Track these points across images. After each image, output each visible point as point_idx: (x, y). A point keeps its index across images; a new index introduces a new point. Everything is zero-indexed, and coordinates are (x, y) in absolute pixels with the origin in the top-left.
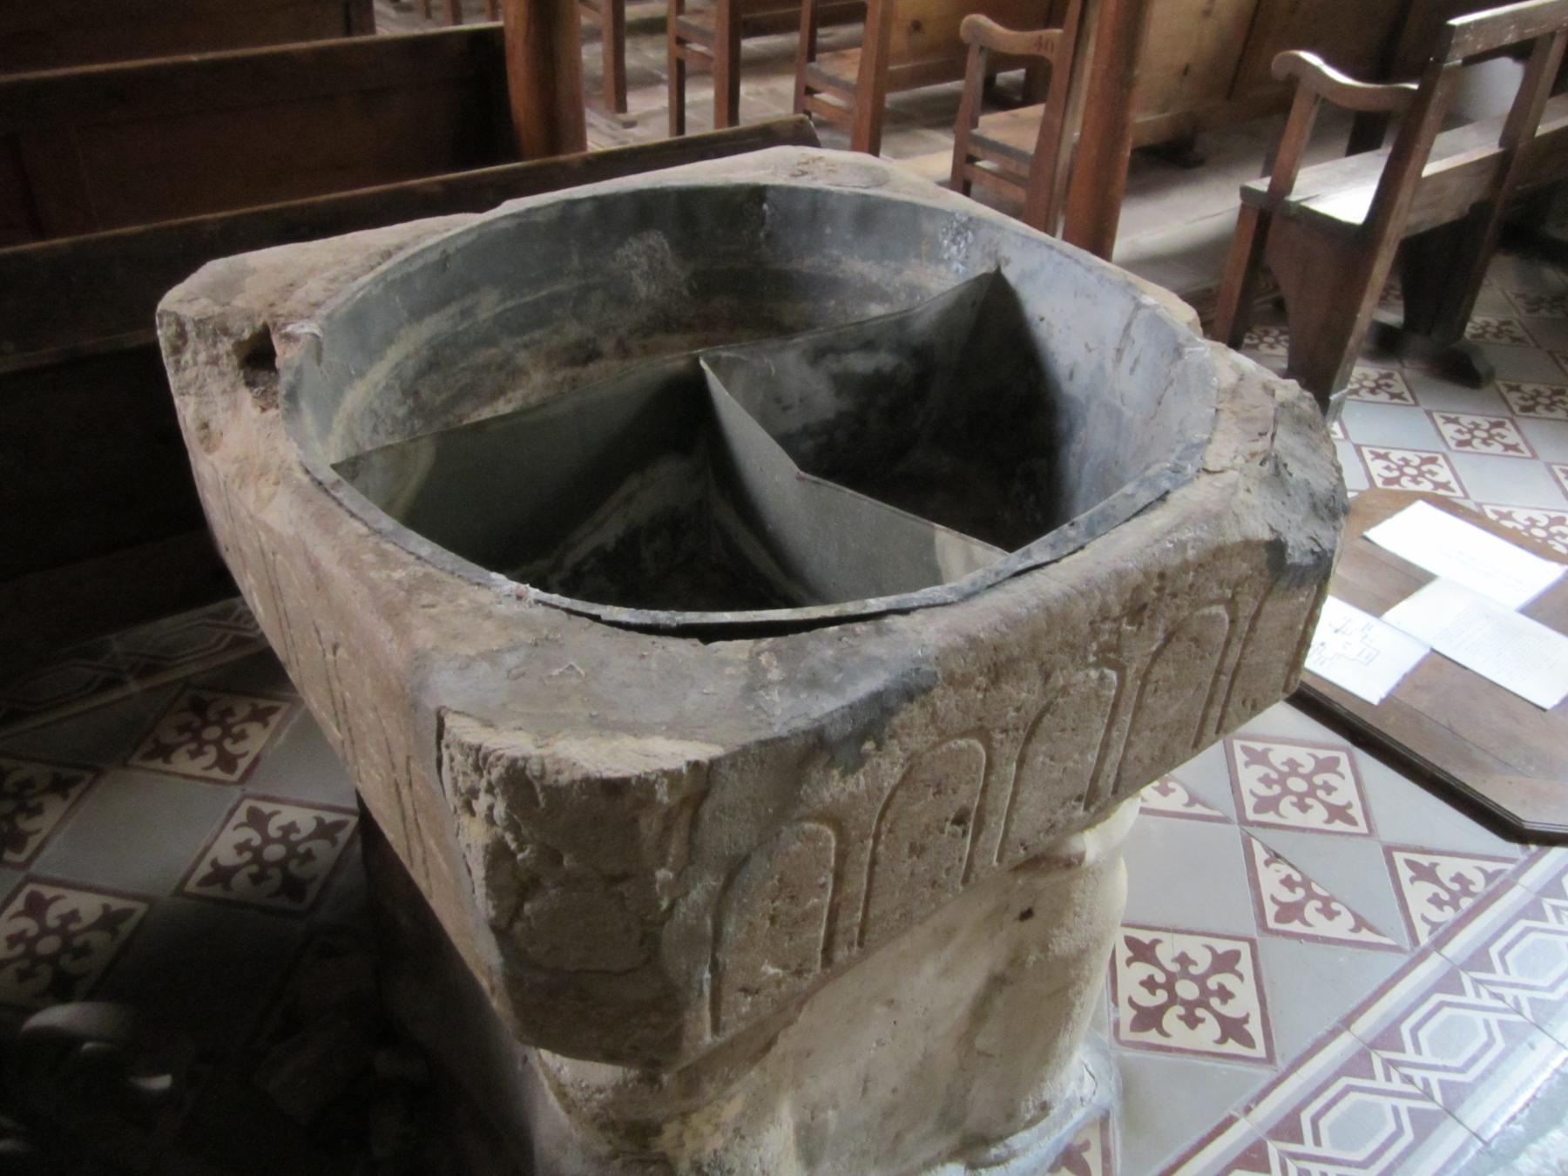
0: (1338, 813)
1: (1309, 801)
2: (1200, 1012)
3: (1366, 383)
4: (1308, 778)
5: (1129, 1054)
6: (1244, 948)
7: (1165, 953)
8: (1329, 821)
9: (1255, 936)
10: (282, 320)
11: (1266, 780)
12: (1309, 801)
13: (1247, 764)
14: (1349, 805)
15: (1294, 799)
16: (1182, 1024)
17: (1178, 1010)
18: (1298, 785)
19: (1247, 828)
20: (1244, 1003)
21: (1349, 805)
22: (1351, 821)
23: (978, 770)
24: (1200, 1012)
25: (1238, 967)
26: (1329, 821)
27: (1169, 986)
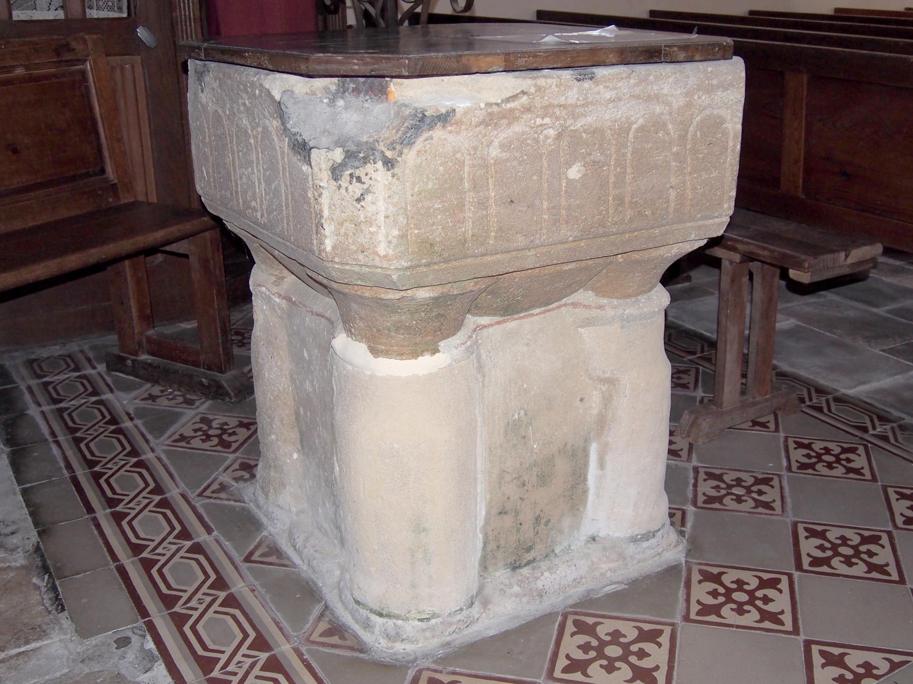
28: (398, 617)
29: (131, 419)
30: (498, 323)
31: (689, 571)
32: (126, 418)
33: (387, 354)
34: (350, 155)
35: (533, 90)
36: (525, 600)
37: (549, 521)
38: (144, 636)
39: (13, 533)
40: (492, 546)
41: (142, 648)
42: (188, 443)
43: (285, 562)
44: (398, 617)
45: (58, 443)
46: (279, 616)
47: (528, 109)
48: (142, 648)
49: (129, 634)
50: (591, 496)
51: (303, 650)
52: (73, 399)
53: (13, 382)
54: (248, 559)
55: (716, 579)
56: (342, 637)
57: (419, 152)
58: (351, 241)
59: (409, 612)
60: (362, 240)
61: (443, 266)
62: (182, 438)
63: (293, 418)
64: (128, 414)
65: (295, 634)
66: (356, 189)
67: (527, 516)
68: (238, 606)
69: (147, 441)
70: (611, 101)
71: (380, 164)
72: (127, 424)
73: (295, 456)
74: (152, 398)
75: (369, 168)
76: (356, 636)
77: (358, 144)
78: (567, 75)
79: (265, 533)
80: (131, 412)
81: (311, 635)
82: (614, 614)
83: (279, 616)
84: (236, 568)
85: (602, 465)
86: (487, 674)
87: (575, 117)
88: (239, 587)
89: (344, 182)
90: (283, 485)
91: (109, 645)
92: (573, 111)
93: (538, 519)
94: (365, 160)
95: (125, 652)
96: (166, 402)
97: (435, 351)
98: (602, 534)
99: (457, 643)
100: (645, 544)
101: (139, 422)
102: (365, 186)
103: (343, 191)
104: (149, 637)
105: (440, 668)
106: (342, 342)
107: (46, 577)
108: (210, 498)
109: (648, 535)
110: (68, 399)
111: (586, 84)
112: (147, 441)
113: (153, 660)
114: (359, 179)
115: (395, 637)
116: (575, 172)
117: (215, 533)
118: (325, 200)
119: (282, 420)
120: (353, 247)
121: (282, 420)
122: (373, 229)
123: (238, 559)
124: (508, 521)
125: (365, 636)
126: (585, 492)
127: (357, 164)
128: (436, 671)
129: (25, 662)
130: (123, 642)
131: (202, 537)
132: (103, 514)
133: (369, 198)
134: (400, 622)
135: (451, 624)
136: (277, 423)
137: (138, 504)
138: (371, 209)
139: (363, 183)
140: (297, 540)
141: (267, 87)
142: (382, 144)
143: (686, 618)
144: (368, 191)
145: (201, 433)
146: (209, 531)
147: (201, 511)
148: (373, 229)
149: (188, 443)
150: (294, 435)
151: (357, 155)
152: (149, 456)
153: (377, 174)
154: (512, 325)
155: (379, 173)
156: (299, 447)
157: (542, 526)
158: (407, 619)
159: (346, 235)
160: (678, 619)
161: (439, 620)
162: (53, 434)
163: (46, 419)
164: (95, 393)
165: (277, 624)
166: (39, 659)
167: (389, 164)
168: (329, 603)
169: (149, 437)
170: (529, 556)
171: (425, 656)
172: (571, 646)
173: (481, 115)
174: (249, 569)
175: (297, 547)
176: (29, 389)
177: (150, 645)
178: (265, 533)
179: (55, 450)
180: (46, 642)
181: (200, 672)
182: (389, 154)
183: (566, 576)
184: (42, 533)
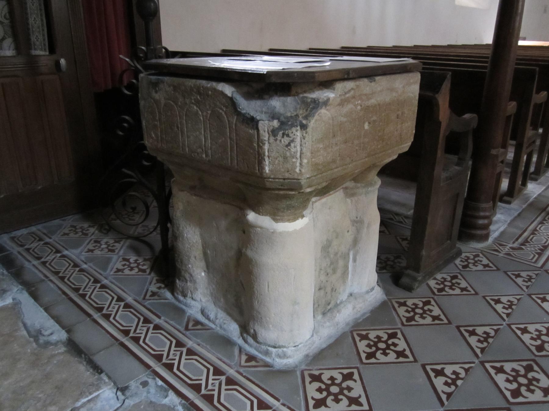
0: (401, 354)
1: (387, 351)
2: (340, 397)
3: (389, 263)
4: (386, 342)
5: (299, 374)
6: (355, 371)
7: (325, 378)
8: (397, 358)
9: (358, 366)
10: (18, 292)
11: (369, 346)
12: (387, 351)
13: (360, 341)
14: (404, 350)
15: (381, 352)
16: (334, 403)
17: (332, 397)
18: (382, 345)
19: (350, 334)
20: (357, 391)
21: (404, 350)
22: (407, 357)
23: (228, 159)
24: (340, 397)
25: (354, 378)
26: (397, 358)
27: (327, 389)
28: (284, 347)
29: (86, 263)
30: (319, 200)
31: (392, 303)
32: (81, 263)
33: (282, 220)
34: (282, 123)
35: (355, 87)
36: (332, 328)
37: (336, 290)
38: (155, 379)
39: (52, 334)
40: (316, 306)
41: (157, 386)
42: (123, 272)
43: (208, 328)
44: (284, 347)
45: (51, 281)
46: (220, 356)
47: (354, 97)
48: (157, 386)
49: (146, 379)
50: (350, 276)
51: (241, 370)
52: (47, 256)
53: (8, 251)
54: (187, 329)
55: (404, 304)
56: (257, 361)
57: (316, 120)
58: (281, 167)
59: (289, 343)
60: (289, 166)
61: (320, 175)
62: (118, 270)
63: (202, 255)
64: (83, 261)
65: (233, 364)
66: (286, 140)
67: (329, 289)
68: (195, 354)
69: (101, 274)
70: (381, 91)
71: (299, 128)
72: (84, 266)
73: (203, 274)
74: (92, 251)
75: (294, 129)
76: (262, 360)
77: (287, 118)
78: (366, 80)
79: (188, 314)
80: (84, 260)
81: (240, 363)
82: (372, 328)
83: (220, 356)
84: (183, 334)
85: (355, 260)
86: (334, 367)
87: (369, 99)
88: (190, 344)
89: (279, 137)
90: (196, 289)
91: (138, 387)
92: (368, 97)
93: (332, 289)
94: (293, 126)
95: (149, 389)
96: (99, 253)
97: (303, 216)
98: (355, 292)
99: (311, 354)
100: (371, 293)
101: (91, 264)
102: (291, 139)
103: (278, 142)
104: (157, 379)
105: (310, 368)
106: (252, 216)
107: (83, 356)
108: (150, 300)
109: (373, 289)
110: (45, 256)
111: (373, 84)
112: (101, 274)
113: (166, 391)
114: (288, 136)
115: (284, 356)
116: (366, 126)
117: (162, 318)
118: (266, 147)
119: (195, 257)
120: (283, 170)
121: (195, 257)
122: (294, 160)
123: (182, 329)
124: (322, 292)
125: (268, 359)
126: (348, 274)
127: (287, 128)
128: (310, 370)
129: (95, 405)
130: (145, 384)
131: (157, 321)
132: (96, 316)
133: (292, 145)
134: (285, 349)
135: (306, 346)
136: (192, 259)
137: (114, 308)
138: (293, 150)
139: (290, 137)
140: (210, 316)
141: (220, 89)
142: (300, 117)
143: (403, 324)
144: (292, 141)
145: (126, 267)
146: (159, 317)
147: (149, 307)
148: (294, 160)
149: (123, 272)
150: (203, 264)
151: (285, 124)
152: (105, 282)
153: (297, 133)
154: (324, 200)
155: (299, 132)
156: (205, 269)
157: (334, 292)
158: (288, 348)
159: (279, 164)
160: (400, 326)
161: (302, 345)
162: (46, 276)
163: (37, 268)
164: (58, 251)
165: (221, 360)
166: (102, 402)
167: (304, 127)
168: (241, 345)
169: (102, 273)
170: (329, 307)
171: (301, 363)
172: (362, 345)
173: (338, 100)
174: (190, 334)
175: (211, 319)
176: (19, 253)
177: (160, 383)
178: (188, 314)
179: (52, 285)
180: (100, 391)
181: (195, 393)
182: (304, 122)
183: (346, 315)
184: (68, 331)
